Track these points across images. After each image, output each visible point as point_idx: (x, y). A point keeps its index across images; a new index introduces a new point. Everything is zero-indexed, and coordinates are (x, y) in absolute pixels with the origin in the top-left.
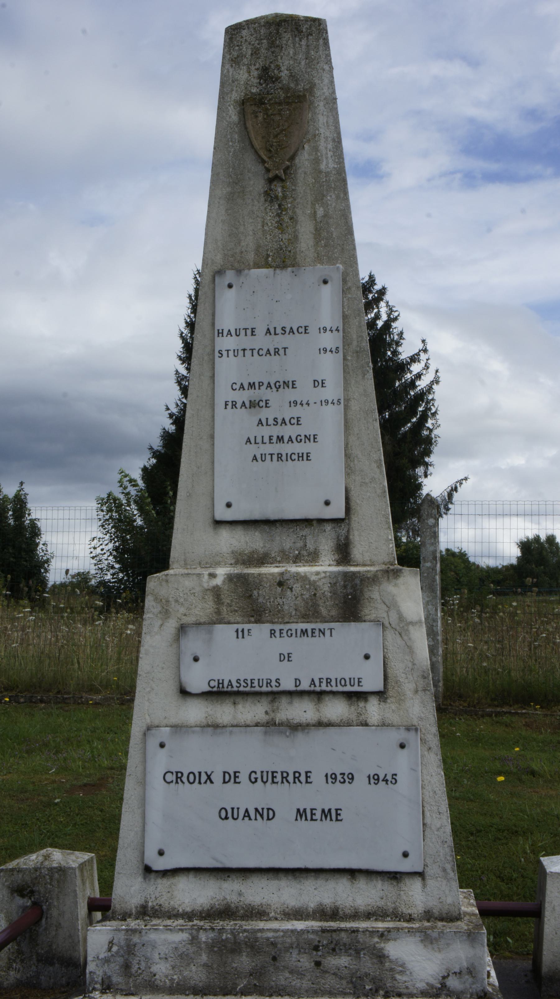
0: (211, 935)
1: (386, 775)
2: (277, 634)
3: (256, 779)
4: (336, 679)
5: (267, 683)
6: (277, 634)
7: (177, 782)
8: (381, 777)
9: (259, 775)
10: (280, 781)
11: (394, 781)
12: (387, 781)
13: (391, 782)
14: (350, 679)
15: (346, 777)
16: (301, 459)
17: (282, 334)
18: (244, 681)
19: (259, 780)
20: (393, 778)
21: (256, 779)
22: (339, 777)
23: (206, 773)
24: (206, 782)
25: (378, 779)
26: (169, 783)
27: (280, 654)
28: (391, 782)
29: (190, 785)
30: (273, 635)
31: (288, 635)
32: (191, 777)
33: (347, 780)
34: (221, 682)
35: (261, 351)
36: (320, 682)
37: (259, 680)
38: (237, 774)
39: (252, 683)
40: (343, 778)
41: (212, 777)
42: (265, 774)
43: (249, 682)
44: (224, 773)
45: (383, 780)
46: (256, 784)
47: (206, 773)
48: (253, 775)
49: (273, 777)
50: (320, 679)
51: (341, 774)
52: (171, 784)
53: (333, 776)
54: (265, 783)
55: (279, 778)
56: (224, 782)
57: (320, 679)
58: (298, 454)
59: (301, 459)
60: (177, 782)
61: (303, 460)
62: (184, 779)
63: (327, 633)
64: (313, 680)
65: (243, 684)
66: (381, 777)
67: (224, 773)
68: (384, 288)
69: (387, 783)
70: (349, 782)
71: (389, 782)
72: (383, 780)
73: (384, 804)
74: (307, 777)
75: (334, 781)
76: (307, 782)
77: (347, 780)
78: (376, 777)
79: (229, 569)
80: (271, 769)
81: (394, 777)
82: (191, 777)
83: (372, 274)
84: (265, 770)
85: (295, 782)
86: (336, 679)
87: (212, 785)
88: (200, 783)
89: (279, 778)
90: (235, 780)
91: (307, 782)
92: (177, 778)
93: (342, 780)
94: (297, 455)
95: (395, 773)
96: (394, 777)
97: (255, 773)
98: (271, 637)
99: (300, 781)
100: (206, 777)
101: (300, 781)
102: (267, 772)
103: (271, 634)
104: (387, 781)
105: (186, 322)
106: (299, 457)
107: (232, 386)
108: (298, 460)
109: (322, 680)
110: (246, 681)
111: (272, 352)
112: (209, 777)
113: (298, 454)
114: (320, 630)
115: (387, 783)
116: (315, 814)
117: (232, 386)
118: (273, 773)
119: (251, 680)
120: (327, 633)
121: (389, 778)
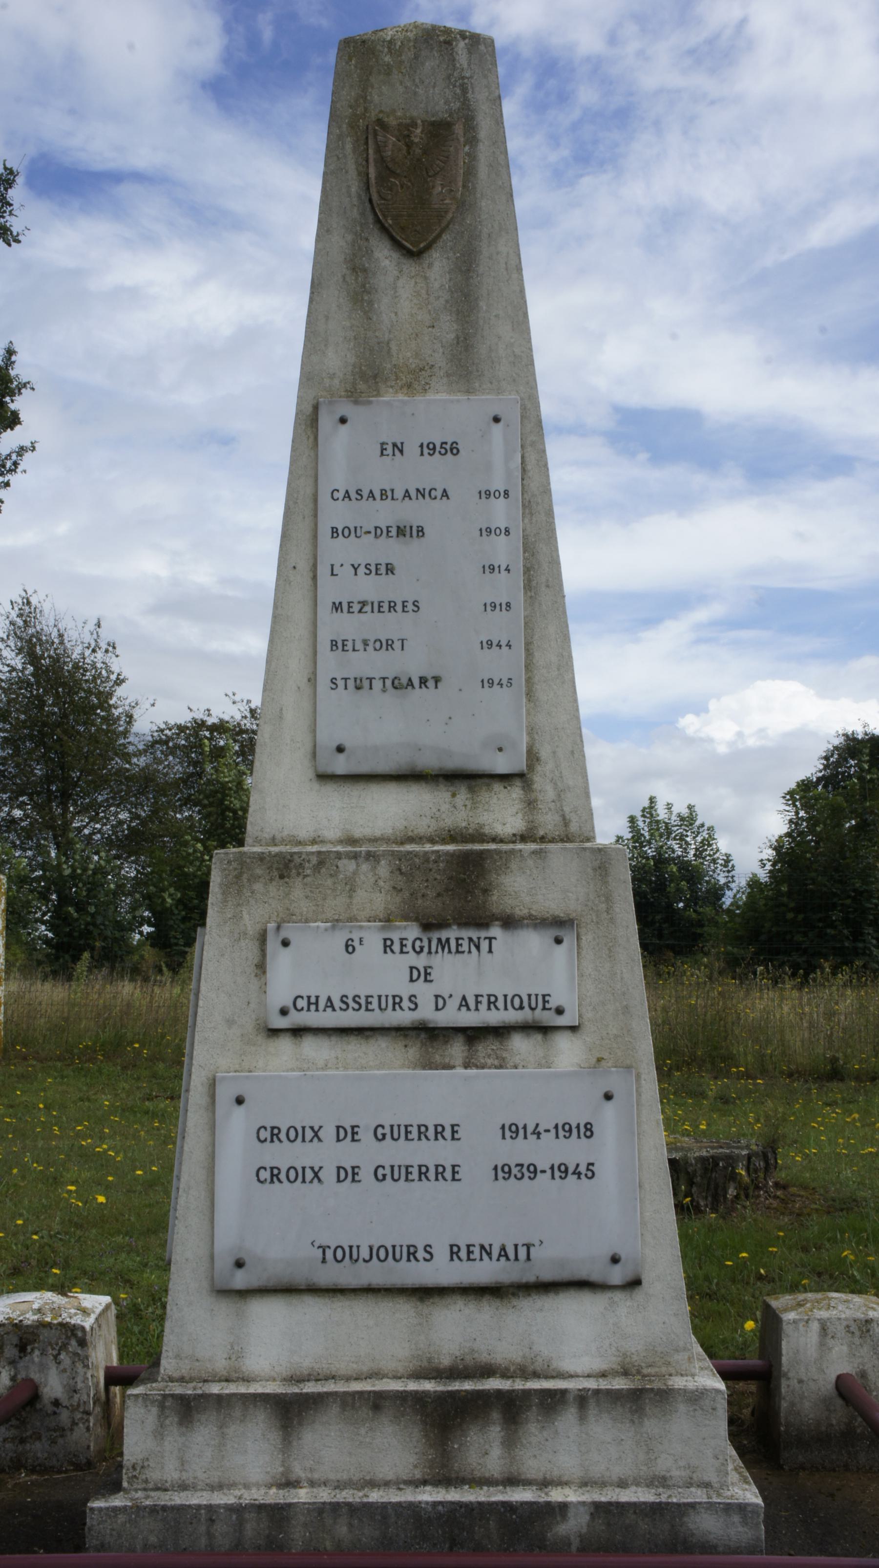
1: (578, 1165)
2: (396, 947)
3: (384, 1176)
4: (505, 996)
6: (396, 947)
7: (272, 1141)
8: (571, 1169)
9: (387, 1130)
10: (416, 1137)
12: (579, 1174)
13: (586, 1175)
14: (529, 996)
16: (313, 1007)
17: (413, 611)
20: (588, 1169)
22: (515, 1171)
24: (311, 1141)
25: (566, 1171)
26: (262, 1182)
28: (586, 1175)
29: (289, 1184)
34: (313, 1000)
35: (335, 492)
36: (477, 1002)
37: (380, 997)
38: (356, 1130)
41: (320, 1174)
43: (363, 1001)
44: (339, 1168)
46: (383, 1142)
48: (380, 1172)
50: (477, 996)
52: (265, 1144)
55: (415, 1134)
57: (477, 996)
59: (313, 1007)
60: (272, 1141)
61: (317, 1010)
62: (283, 1136)
66: (571, 1169)
67: (339, 1168)
69: (579, 1178)
71: (583, 1176)
73: (566, 1154)
80: (403, 1123)
81: (591, 1167)
84: (395, 1123)
85: (437, 1179)
86: (505, 996)
87: (320, 1143)
88: (304, 1181)
90: (353, 1137)
91: (453, 1138)
94: (306, 999)
95: (591, 1161)
96: (591, 1167)
97: (383, 1127)
99: (443, 1137)
100: (312, 1134)
101: (443, 1137)
102: (399, 1126)
103: (385, 946)
104: (579, 1174)
106: (309, 1003)
107: (257, 1175)
108: (309, 1010)
109: (480, 999)
110: (357, 999)
111: (377, 495)
112: (316, 1175)
113: (309, 997)
114: (471, 939)
115: (579, 1178)
116: (472, 1252)
117: (257, 1175)
118: (407, 1167)
119: (367, 997)
120: (485, 945)
121: (582, 1169)
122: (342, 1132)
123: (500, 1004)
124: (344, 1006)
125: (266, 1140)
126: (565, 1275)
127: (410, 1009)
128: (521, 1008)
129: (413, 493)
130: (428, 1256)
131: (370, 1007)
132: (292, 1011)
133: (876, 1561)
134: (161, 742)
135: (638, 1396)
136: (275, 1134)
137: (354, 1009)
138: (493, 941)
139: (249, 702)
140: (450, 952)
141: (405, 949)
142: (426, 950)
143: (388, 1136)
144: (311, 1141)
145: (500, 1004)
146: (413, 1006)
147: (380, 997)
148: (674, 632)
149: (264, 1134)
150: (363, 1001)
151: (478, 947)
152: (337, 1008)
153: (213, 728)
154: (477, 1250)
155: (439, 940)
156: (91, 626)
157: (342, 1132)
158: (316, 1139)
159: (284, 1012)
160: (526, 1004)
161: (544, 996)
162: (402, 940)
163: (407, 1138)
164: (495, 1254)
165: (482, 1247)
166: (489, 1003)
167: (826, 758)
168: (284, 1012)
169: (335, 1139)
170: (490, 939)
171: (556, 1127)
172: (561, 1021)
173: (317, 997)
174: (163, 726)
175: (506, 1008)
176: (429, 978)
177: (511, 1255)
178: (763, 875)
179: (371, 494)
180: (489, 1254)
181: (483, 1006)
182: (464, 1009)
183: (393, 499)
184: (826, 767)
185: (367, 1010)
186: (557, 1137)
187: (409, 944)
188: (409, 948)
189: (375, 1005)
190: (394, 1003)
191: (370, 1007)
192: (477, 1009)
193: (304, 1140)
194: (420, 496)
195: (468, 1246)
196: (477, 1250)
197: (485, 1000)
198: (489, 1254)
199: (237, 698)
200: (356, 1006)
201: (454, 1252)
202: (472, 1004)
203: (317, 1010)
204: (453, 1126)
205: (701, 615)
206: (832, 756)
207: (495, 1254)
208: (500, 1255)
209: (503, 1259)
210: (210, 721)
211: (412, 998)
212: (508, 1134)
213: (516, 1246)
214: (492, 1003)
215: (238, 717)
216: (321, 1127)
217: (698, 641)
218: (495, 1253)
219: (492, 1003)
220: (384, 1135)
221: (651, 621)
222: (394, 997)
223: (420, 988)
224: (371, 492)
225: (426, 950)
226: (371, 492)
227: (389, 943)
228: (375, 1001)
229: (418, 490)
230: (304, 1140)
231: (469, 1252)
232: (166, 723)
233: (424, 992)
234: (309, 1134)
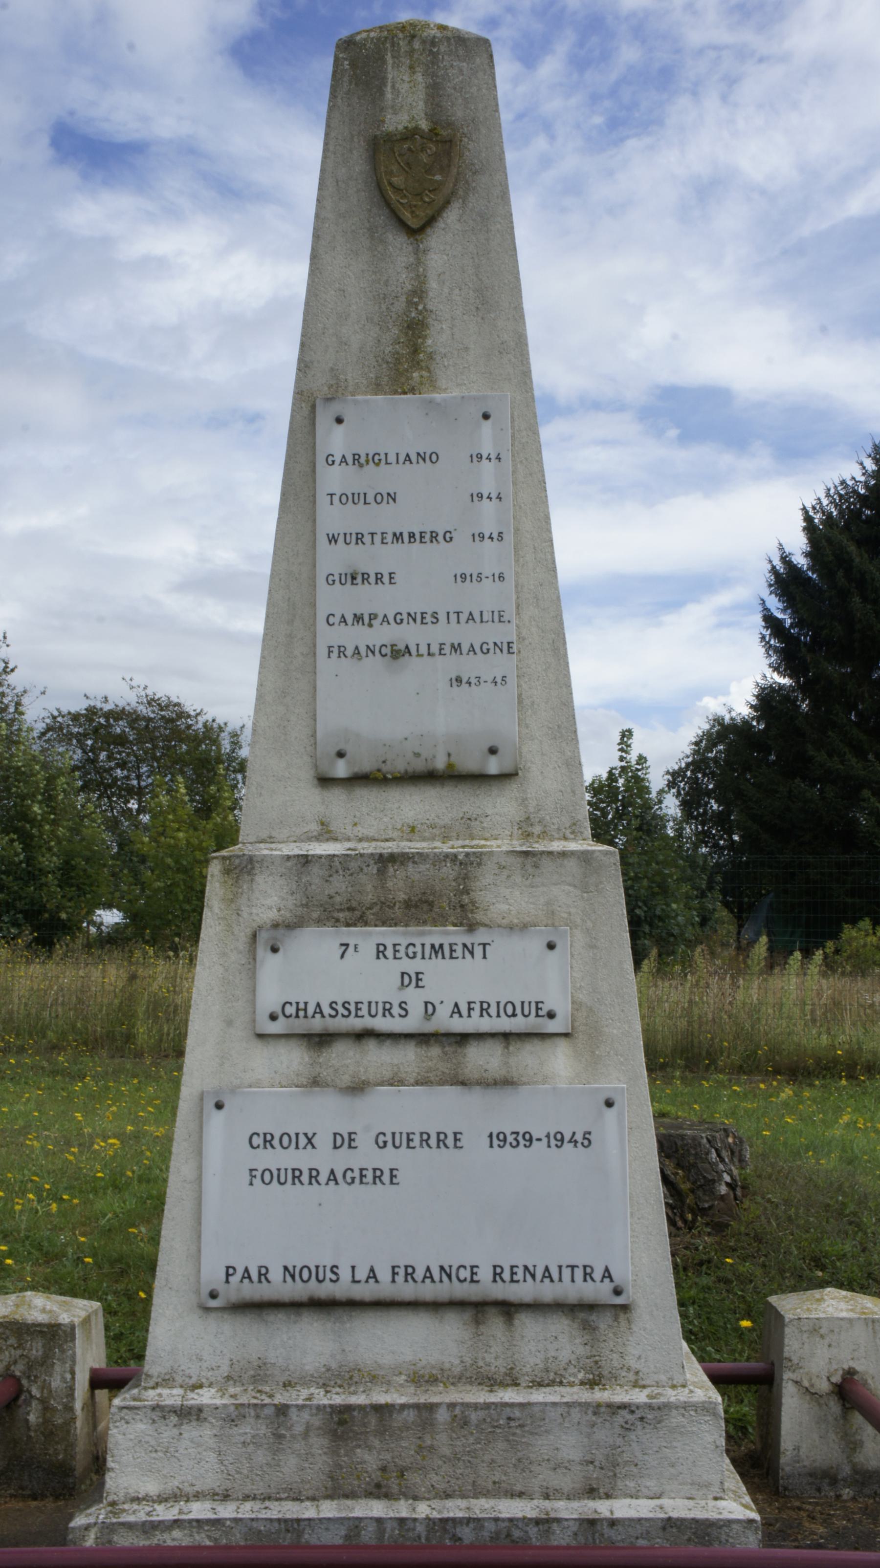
0: (522, 1534)
1: (574, 1133)
2: (389, 952)
5: (384, 1009)
6: (389, 952)
8: (567, 1137)
11: (586, 1142)
15: (520, 1138)
18: (343, 1006)
19: (390, 1144)
20: (584, 1138)
21: (385, 1143)
22: (510, 1139)
23: (306, 1135)
24: (305, 1148)
25: (562, 1140)
27: (403, 974)
30: (381, 955)
31: (407, 955)
33: (522, 1142)
34: (302, 1006)
36: (470, 1009)
37: (370, 1003)
39: (357, 1009)
40: (516, 1139)
41: (313, 1141)
42: (397, 1137)
43: (352, 1008)
45: (570, 1141)
47: (306, 1135)
48: (381, 1139)
50: (469, 1003)
51: (513, 1133)
53: (501, 1137)
55: (416, 1142)
56: (335, 1147)
57: (469, 1003)
58: (298, 1003)
60: (265, 1147)
62: (276, 1142)
63: (478, 951)
64: (456, 1005)
65: (341, 1010)
66: (567, 1137)
69: (575, 1146)
70: (499, 1146)
71: (579, 1145)
72: (570, 1141)
75: (502, 1144)
76: (456, 1146)
77: (522, 1142)
78: (559, 1137)
85: (438, 1147)
86: (498, 1003)
89: (416, 1142)
91: (456, 1146)
92: (265, 1141)
93: (514, 1143)
94: (294, 1005)
97: (384, 1134)
98: (378, 958)
100: (306, 1141)
103: (378, 952)
104: (576, 1142)
105: (774, 570)
110: (403, 1005)
112: (310, 1141)
113: (298, 1003)
114: (465, 945)
115: (575, 1146)
120: (478, 951)
121: (579, 1137)
122: (339, 1139)
123: (493, 1011)
124: (333, 1013)
125: (258, 1146)
127: (400, 1016)
128: (514, 1015)
129: (414, 458)
130: (403, 1013)
131: (360, 1013)
132: (281, 1018)
133: (875, 1556)
134: (56, 729)
136: (268, 1141)
137: (343, 1016)
138: (487, 947)
139: (146, 688)
140: (443, 957)
141: (398, 955)
142: (419, 955)
143: (390, 1144)
144: (305, 1148)
145: (493, 1011)
147: (370, 1003)
148: (696, 616)
149: (257, 1141)
150: (352, 1008)
153: (108, 715)
154: (520, 1272)
155: (433, 946)
157: (339, 1139)
158: (309, 1146)
159: (273, 1017)
160: (518, 1011)
162: (395, 945)
163: (408, 1147)
164: (539, 1276)
165: (526, 1268)
166: (482, 1009)
167: (697, 744)
168: (273, 1017)
169: (332, 1145)
171: (548, 1136)
172: (552, 1027)
173: (306, 1003)
174: (56, 713)
175: (498, 1016)
177: (555, 1276)
180: (533, 1276)
182: (456, 1016)
183: (387, 463)
184: (696, 752)
185: (357, 1016)
186: (549, 1146)
188: (402, 954)
189: (364, 1011)
192: (469, 1016)
193: (297, 1147)
194: (420, 460)
195: (512, 1267)
196: (520, 1272)
197: (477, 1007)
198: (533, 1276)
199: (134, 683)
200: (346, 1013)
201: (497, 1274)
202: (464, 1012)
204: (455, 1134)
205: (724, 598)
206: (701, 741)
207: (539, 1276)
208: (544, 1277)
209: (547, 1281)
210: (107, 707)
211: (402, 1005)
212: (496, 1142)
213: (560, 1267)
214: (484, 1010)
215: (134, 704)
216: (314, 1134)
217: (720, 625)
218: (539, 1275)
219: (484, 1010)
220: (385, 1143)
221: (675, 605)
224: (408, 455)
226: (408, 455)
227: (381, 948)
229: (418, 454)
230: (297, 1147)
231: (513, 1274)
232: (58, 710)
233: (415, 998)
234: (303, 1141)
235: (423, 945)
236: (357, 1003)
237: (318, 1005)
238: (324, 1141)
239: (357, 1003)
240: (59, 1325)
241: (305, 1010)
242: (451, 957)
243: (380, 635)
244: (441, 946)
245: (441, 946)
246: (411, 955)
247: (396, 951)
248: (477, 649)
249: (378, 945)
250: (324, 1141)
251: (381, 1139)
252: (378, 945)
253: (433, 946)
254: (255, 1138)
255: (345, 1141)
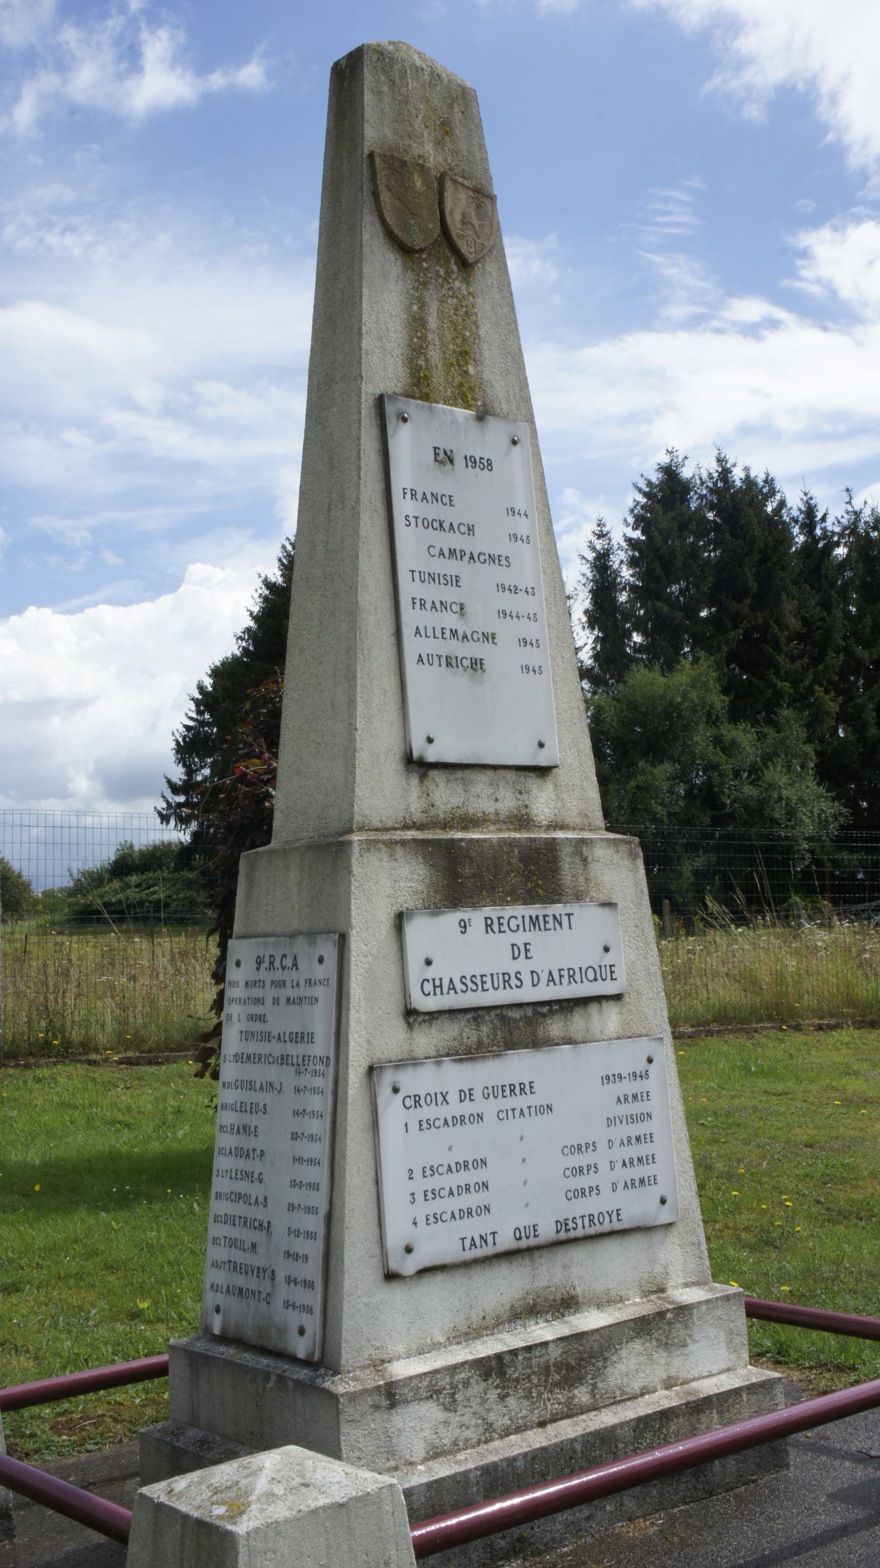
16: (438, 990)
32: (428, 1098)
34: (437, 983)
36: (561, 976)
37: (492, 975)
39: (483, 983)
43: (479, 981)
48: (486, 1092)
49: (503, 1091)
50: (560, 970)
54: (496, 1097)
57: (560, 970)
58: (434, 980)
59: (438, 990)
61: (442, 993)
63: (565, 920)
68: (768, 475)
74: (531, 1087)
79: (366, 236)
82: (428, 1098)
83: (555, 770)
98: (487, 932)
103: (487, 925)
106: (435, 987)
108: (435, 994)
112: (444, 1097)
113: (434, 980)
124: (464, 988)
126: (634, 1225)
130: (519, 983)
135: (661, 1325)
142: (521, 928)
146: (519, 983)
147: (492, 975)
151: (560, 924)
152: (458, 990)
155: (531, 917)
156: (581, 578)
161: (611, 966)
162: (499, 918)
170: (569, 915)
173: (441, 979)
176: (529, 955)
178: (136, 848)
179: (424, 497)
181: (565, 980)
182: (551, 984)
185: (483, 990)
187: (505, 922)
190: (504, 981)
191: (485, 987)
200: (474, 987)
203: (442, 993)
222: (504, 974)
223: (523, 965)
225: (521, 928)
228: (488, 979)
234: (440, 1098)
235: (523, 917)
236: (482, 976)
237: (451, 981)
238: (453, 1097)
239: (482, 976)
240: (368, 1494)
241: (441, 986)
242: (546, 929)
243: (276, 1048)
244: (537, 917)
245: (537, 917)
246: (514, 928)
247: (500, 924)
248: (469, 637)
249: (486, 919)
250: (453, 1097)
251: (486, 1092)
252: (486, 919)
253: (531, 917)
254: (407, 1099)
255: (466, 1095)
